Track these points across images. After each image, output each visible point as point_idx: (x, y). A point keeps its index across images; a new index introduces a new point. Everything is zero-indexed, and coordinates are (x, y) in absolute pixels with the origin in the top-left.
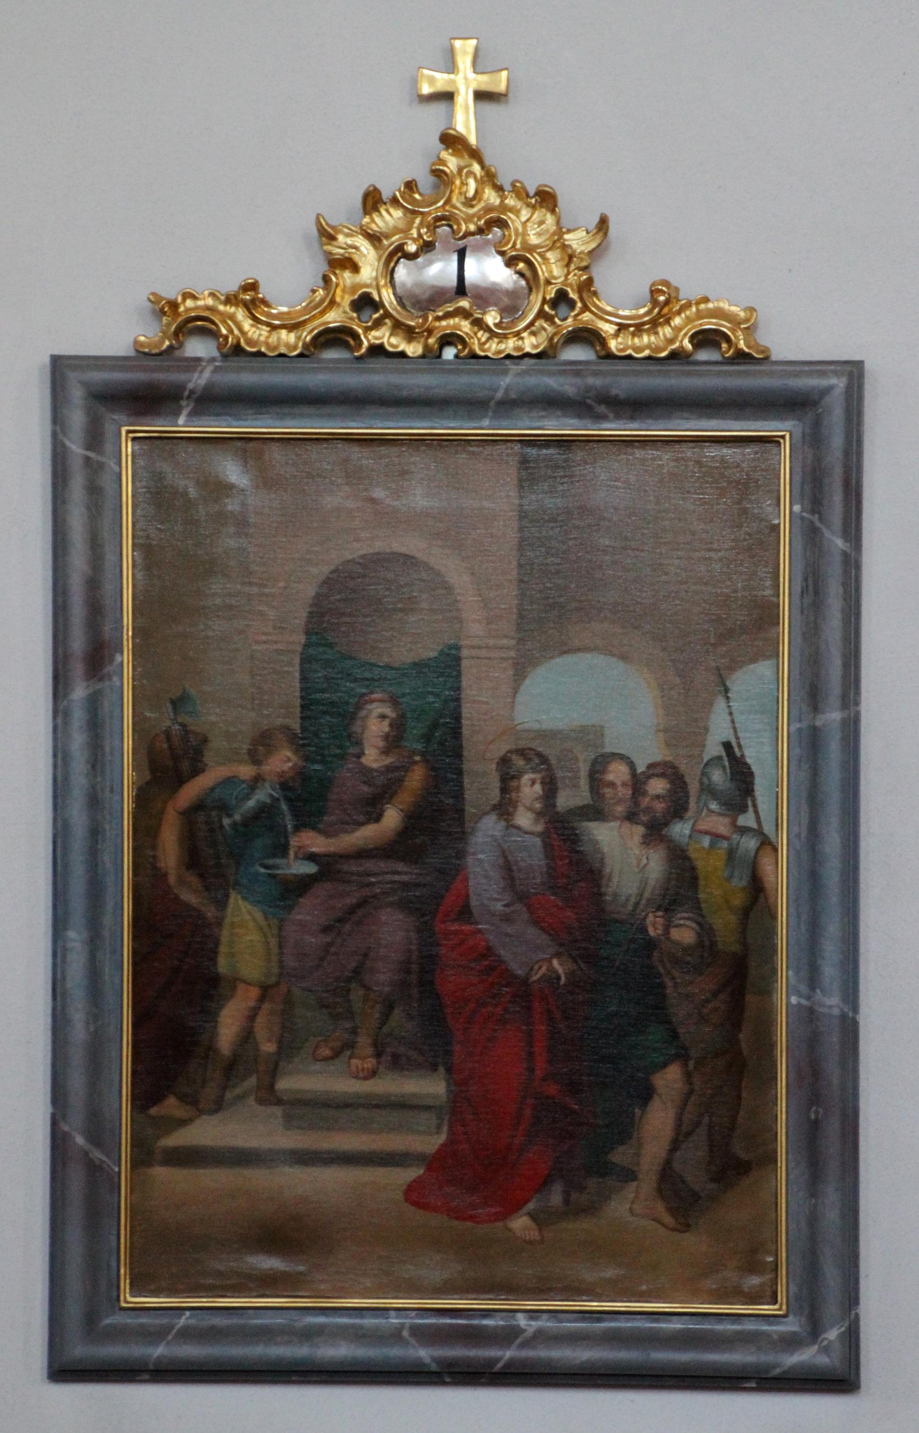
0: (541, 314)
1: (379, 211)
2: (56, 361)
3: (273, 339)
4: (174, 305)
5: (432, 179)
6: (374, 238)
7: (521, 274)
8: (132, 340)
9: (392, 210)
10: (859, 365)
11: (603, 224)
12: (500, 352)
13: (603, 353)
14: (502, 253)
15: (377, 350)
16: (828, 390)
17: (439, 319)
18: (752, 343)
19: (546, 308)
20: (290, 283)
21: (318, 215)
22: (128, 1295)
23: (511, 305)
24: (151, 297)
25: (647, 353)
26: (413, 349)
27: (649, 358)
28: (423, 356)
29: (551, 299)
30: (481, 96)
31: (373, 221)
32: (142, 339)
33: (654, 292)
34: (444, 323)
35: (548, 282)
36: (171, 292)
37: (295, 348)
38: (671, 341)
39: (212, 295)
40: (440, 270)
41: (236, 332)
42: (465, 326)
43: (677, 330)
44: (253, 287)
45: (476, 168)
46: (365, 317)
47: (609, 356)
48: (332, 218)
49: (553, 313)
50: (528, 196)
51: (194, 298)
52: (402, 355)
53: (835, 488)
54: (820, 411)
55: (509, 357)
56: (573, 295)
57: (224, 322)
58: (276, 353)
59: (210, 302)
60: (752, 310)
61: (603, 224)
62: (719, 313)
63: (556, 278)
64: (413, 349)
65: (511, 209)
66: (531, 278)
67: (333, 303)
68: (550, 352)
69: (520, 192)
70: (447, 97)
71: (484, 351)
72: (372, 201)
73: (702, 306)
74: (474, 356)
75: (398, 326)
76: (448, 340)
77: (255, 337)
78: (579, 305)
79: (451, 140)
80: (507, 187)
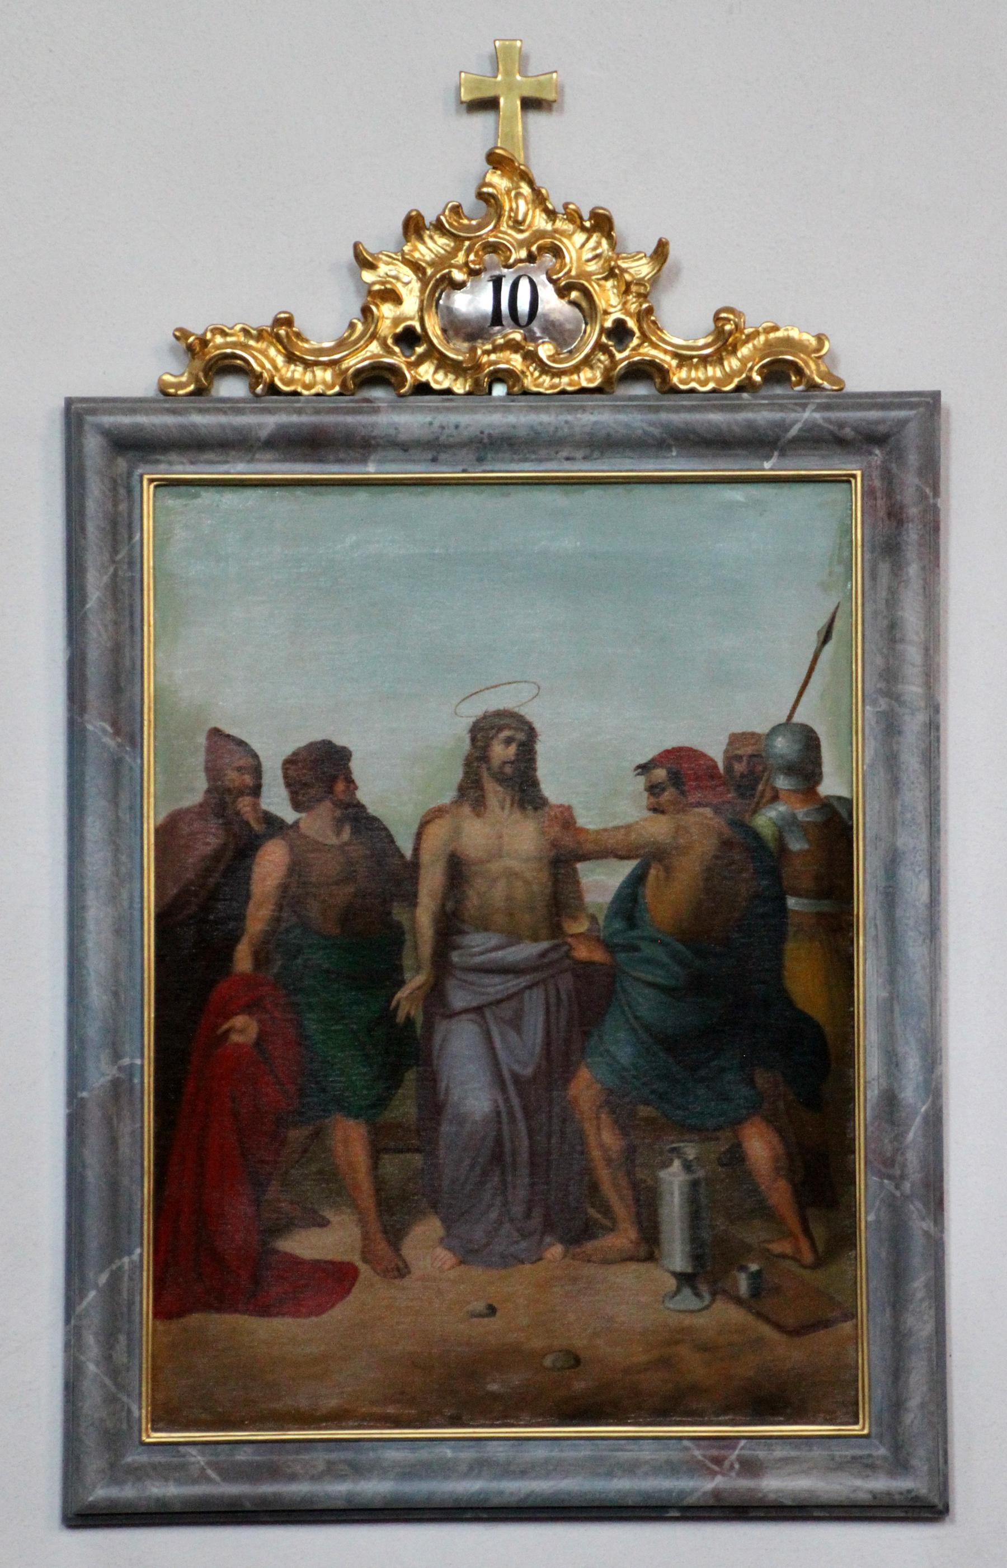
0: (599, 347)
2: (69, 402)
3: (308, 377)
4: (204, 342)
5: (483, 204)
6: (416, 267)
7: (574, 303)
8: (156, 381)
9: (436, 237)
10: (936, 396)
11: (661, 252)
13: (666, 388)
15: (423, 389)
16: (903, 423)
17: (488, 353)
19: (604, 339)
21: (356, 246)
23: (556, 332)
24: (177, 334)
25: (711, 386)
26: (460, 387)
27: (714, 391)
28: (469, 393)
31: (415, 249)
33: (717, 318)
35: (606, 313)
36: (197, 328)
37: (333, 386)
40: (474, 301)
41: (268, 366)
42: (516, 361)
43: (743, 361)
44: (289, 322)
45: (525, 189)
47: (675, 391)
48: (370, 246)
50: (581, 218)
51: (224, 334)
52: (448, 392)
53: (904, 529)
54: (890, 453)
55: (563, 392)
56: (631, 324)
58: (313, 391)
61: (661, 252)
62: (788, 343)
64: (460, 387)
65: (562, 233)
66: (588, 308)
67: (374, 336)
68: (607, 389)
69: (574, 217)
71: (537, 386)
72: (414, 226)
73: (772, 335)
74: (526, 393)
75: (444, 363)
78: (638, 334)
80: (560, 209)
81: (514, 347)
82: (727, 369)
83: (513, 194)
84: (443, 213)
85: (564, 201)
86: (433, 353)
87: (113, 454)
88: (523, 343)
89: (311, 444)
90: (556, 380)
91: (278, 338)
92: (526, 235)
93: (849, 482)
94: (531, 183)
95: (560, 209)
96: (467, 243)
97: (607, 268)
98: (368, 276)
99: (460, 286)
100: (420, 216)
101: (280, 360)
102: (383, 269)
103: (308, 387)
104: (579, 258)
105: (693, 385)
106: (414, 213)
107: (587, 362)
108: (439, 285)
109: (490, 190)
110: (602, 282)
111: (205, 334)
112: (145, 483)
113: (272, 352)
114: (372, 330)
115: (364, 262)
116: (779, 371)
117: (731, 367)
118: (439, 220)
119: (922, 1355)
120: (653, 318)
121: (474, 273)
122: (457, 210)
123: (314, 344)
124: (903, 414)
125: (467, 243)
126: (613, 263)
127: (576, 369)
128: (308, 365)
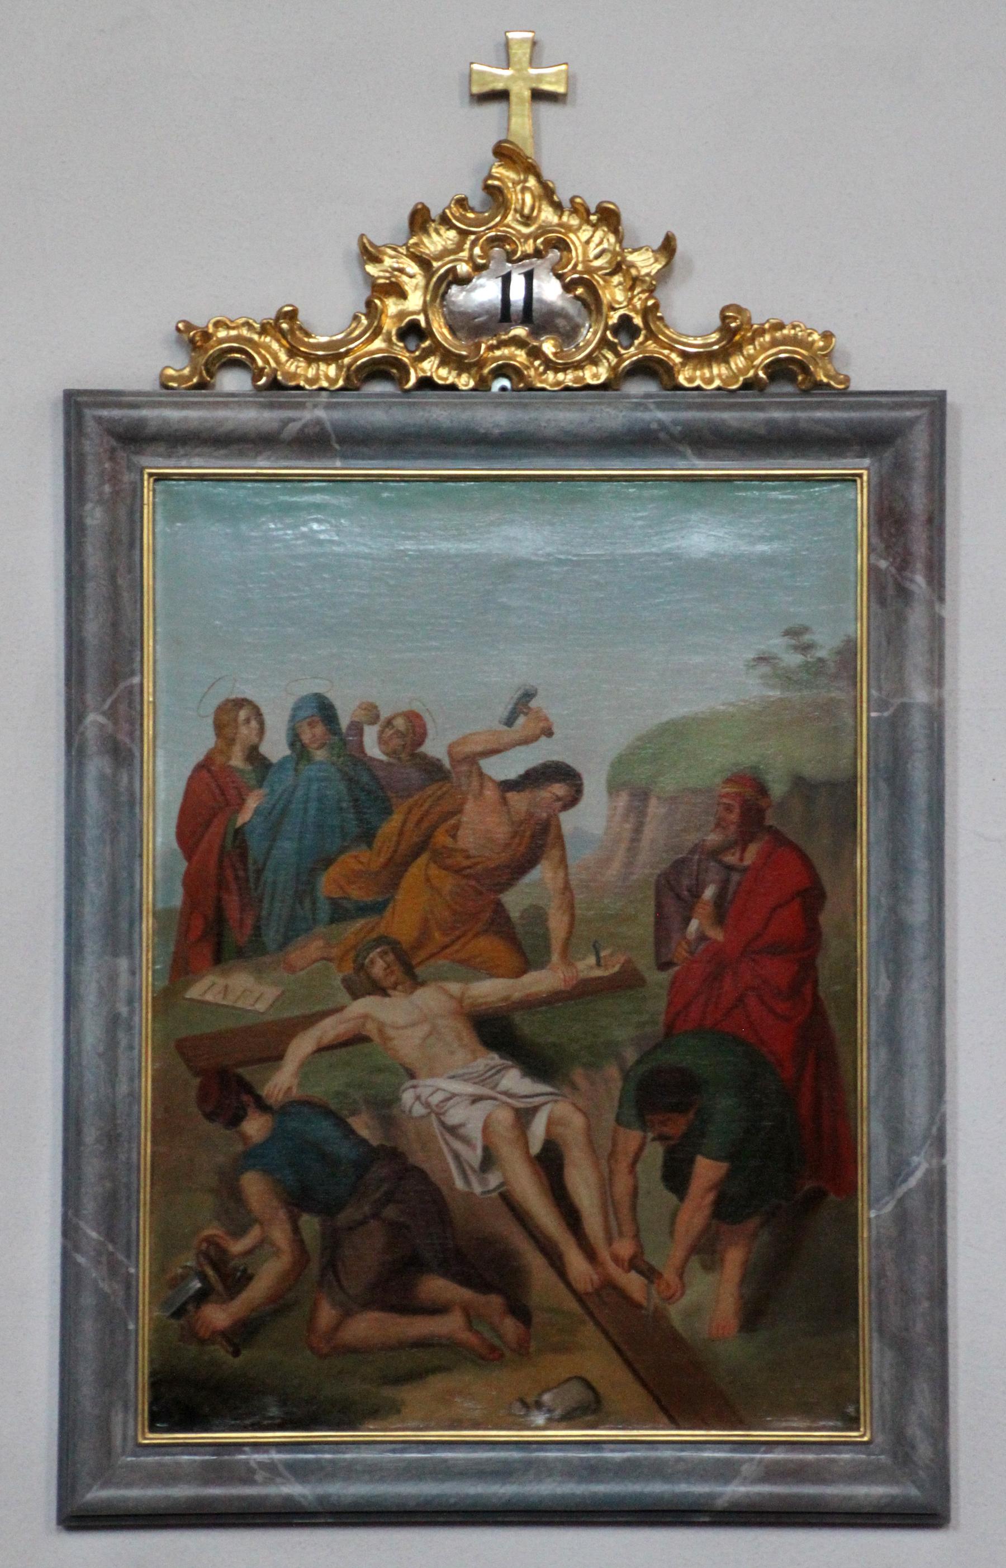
1: (429, 235)
4: (206, 336)
5: (490, 198)
6: (424, 263)
10: (941, 397)
11: (668, 247)
12: (558, 383)
14: (560, 277)
15: (426, 383)
16: (912, 423)
17: (491, 348)
18: (832, 373)
19: (608, 333)
20: (330, 312)
22: (146, 1430)
24: (180, 326)
25: (717, 383)
26: (465, 382)
27: (719, 388)
28: (473, 390)
29: (614, 325)
30: (539, 96)
32: (170, 372)
33: (724, 318)
34: (498, 353)
38: (742, 371)
39: (248, 325)
40: (485, 292)
41: (273, 364)
42: (521, 356)
43: (750, 358)
44: (292, 316)
45: (532, 182)
46: (412, 346)
47: (680, 387)
48: (377, 238)
49: (616, 341)
50: (588, 213)
52: (453, 387)
53: (909, 539)
54: (893, 449)
56: (638, 321)
57: (259, 353)
59: (244, 332)
60: (827, 336)
62: (794, 341)
63: (620, 303)
65: (569, 228)
67: (377, 332)
70: (502, 96)
71: (541, 382)
72: (420, 220)
73: (778, 334)
74: (531, 388)
75: (448, 358)
76: (500, 372)
77: (293, 369)
79: (505, 153)
80: (566, 204)
81: (518, 342)
82: (733, 366)
83: (519, 187)
84: (449, 207)
85: (570, 196)
86: (437, 349)
87: (108, 444)
88: (528, 340)
89: (313, 442)
90: (561, 376)
91: (281, 331)
92: (532, 229)
93: (855, 481)
94: (538, 177)
95: (566, 204)
96: (473, 237)
97: (614, 263)
98: (371, 269)
99: (463, 281)
100: (428, 210)
101: (283, 357)
102: (388, 262)
103: (308, 381)
104: (585, 253)
105: (698, 382)
106: (420, 206)
107: (592, 360)
108: (443, 283)
109: (496, 183)
110: (607, 277)
111: (207, 327)
112: (146, 477)
113: (275, 346)
114: (375, 324)
115: (370, 254)
116: (780, 370)
117: (736, 365)
118: (444, 213)
119: (925, 1353)
120: (659, 314)
121: (479, 269)
122: (462, 203)
123: (324, 339)
124: (909, 414)
125: (473, 237)
126: (619, 258)
127: (579, 366)
128: (311, 359)
